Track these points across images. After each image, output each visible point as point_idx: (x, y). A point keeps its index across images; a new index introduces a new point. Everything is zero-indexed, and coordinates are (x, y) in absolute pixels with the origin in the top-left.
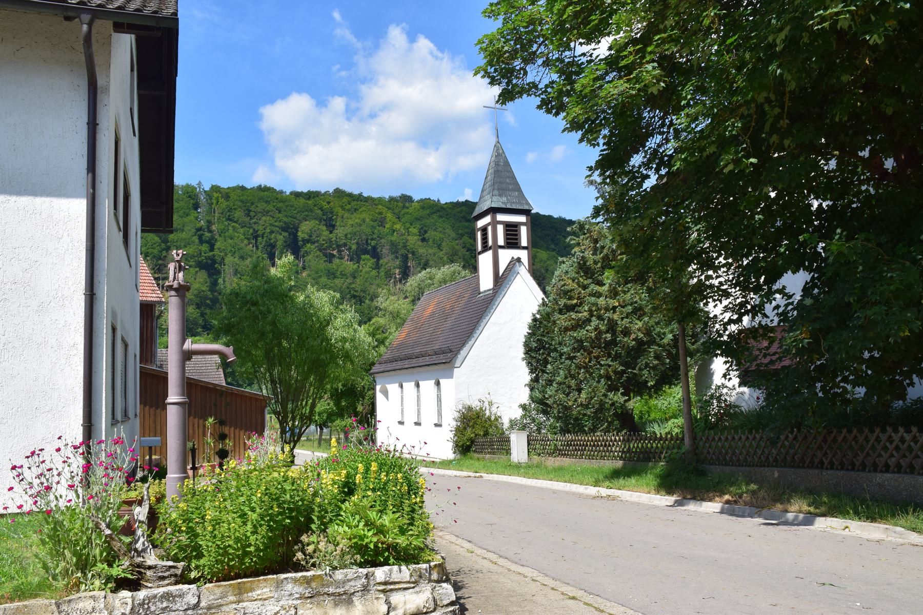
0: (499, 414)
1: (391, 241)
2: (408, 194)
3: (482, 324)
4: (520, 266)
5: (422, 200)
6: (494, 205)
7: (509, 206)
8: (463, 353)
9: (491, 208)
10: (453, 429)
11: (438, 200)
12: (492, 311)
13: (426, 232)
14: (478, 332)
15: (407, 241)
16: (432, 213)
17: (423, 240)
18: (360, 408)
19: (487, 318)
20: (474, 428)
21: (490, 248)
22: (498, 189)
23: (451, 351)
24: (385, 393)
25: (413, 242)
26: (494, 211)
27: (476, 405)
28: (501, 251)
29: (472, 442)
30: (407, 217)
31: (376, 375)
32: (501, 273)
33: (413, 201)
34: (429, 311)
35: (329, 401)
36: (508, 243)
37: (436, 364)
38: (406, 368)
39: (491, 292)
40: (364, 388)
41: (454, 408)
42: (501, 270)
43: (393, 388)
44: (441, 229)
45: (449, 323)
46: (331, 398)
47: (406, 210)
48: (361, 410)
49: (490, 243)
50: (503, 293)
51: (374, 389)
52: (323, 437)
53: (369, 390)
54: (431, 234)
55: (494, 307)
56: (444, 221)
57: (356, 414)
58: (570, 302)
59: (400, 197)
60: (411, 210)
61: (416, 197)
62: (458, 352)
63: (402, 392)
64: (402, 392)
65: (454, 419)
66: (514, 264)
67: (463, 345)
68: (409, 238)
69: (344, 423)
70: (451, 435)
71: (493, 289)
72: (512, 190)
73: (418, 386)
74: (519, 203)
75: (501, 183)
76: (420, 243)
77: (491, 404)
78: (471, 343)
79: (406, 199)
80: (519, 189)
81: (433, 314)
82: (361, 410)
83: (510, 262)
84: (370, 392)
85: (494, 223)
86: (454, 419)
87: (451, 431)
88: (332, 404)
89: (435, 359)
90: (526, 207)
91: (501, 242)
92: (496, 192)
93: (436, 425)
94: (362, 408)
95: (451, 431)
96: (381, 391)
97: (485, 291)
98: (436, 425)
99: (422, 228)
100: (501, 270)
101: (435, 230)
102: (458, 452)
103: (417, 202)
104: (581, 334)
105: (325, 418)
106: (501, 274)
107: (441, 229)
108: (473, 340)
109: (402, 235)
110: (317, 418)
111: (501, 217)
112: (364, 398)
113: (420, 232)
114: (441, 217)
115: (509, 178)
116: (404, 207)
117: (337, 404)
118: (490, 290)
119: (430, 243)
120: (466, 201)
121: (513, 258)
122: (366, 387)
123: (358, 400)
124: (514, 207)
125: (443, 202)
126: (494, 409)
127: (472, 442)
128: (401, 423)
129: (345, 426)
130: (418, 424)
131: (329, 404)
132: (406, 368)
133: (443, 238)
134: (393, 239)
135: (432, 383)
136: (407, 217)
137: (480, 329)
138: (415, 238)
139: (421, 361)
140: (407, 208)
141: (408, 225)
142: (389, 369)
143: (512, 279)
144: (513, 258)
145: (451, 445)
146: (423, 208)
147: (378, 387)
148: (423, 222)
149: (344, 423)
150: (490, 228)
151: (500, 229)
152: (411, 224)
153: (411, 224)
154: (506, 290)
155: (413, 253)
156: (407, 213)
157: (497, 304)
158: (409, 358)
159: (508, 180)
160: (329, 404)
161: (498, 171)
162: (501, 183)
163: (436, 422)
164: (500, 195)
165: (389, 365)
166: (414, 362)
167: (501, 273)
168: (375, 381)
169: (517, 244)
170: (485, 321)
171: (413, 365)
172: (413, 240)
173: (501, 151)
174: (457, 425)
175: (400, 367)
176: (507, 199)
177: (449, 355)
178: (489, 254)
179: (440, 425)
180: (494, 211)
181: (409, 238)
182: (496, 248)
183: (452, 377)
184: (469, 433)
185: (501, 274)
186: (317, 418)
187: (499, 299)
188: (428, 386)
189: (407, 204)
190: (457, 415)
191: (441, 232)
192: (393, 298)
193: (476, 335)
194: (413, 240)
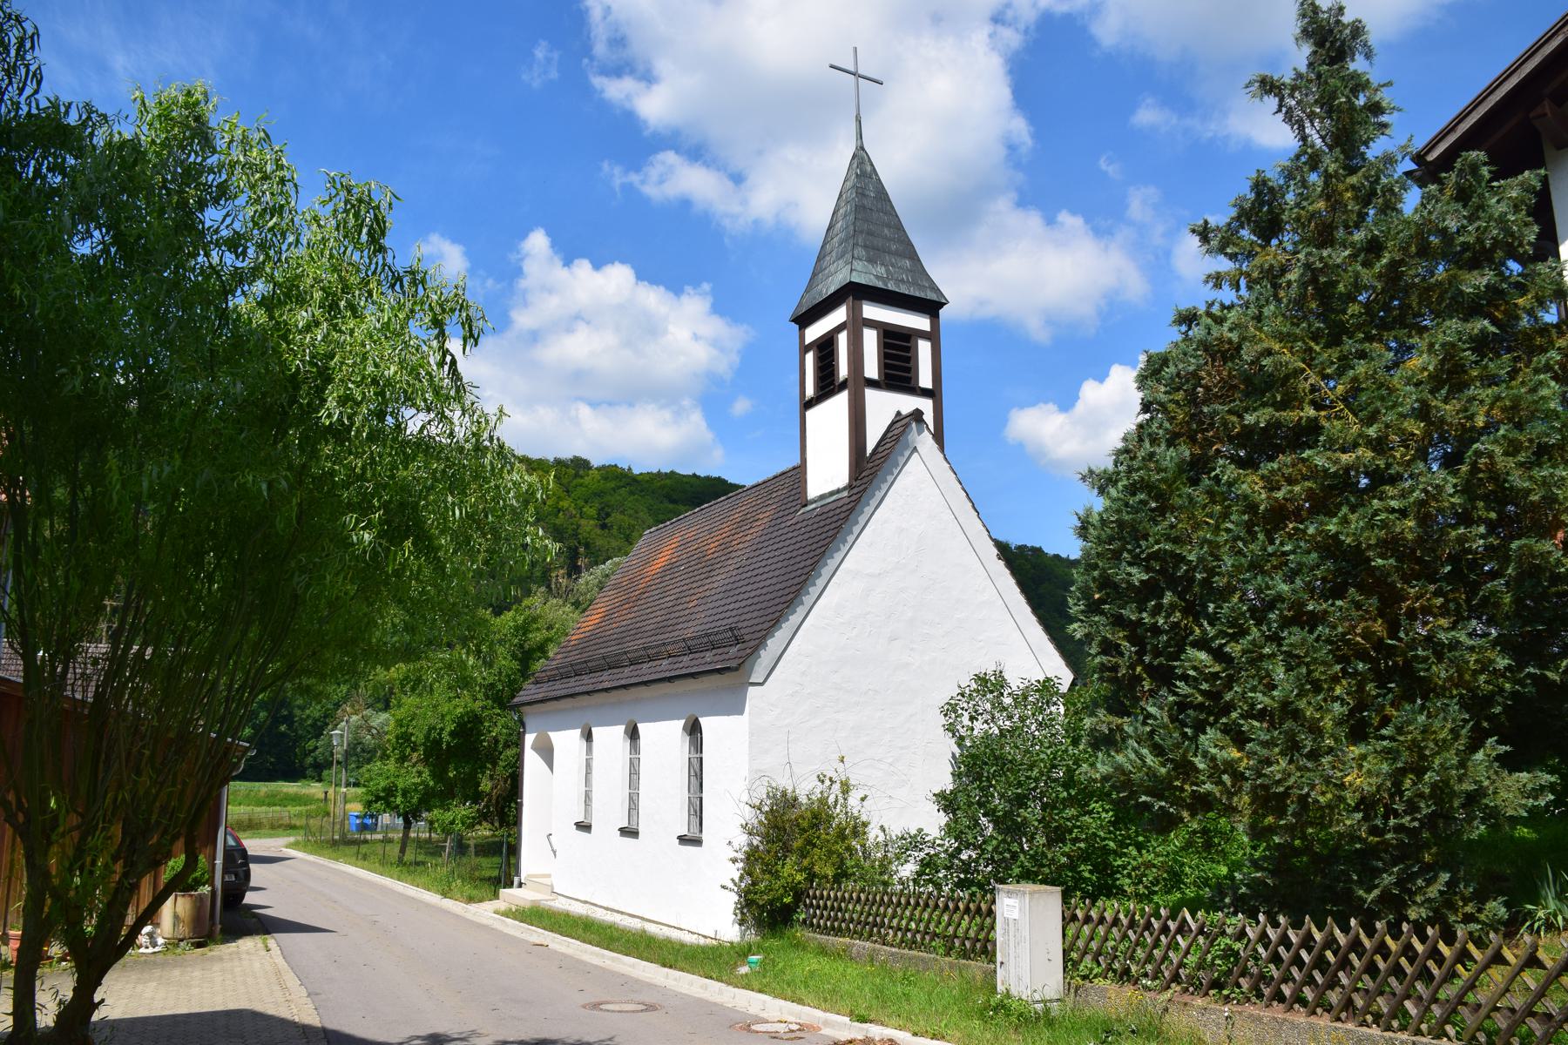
0: (864, 818)
1: (555, 525)
2: (584, 457)
3: (826, 572)
4: (920, 433)
5: (604, 467)
6: (856, 279)
7: (891, 286)
8: (774, 644)
9: (851, 283)
10: (741, 856)
11: (630, 469)
12: (850, 539)
13: (608, 515)
14: (814, 591)
15: (579, 526)
16: (619, 487)
17: (604, 527)
18: (486, 785)
19: (838, 556)
20: (804, 856)
21: (843, 386)
22: (865, 247)
23: (738, 640)
24: (547, 753)
25: (588, 529)
26: (854, 293)
27: (805, 788)
28: (871, 395)
29: (799, 895)
30: (580, 490)
31: (525, 709)
32: (870, 447)
33: (590, 468)
34: (661, 562)
35: (420, 767)
36: (887, 375)
37: (693, 675)
38: (606, 690)
39: (845, 494)
40: (496, 741)
41: (745, 798)
42: (871, 441)
43: (566, 741)
44: (631, 512)
45: (720, 579)
46: (426, 761)
47: (580, 481)
48: (488, 789)
49: (843, 371)
50: (879, 495)
51: (519, 744)
52: (413, 835)
53: (507, 746)
54: (616, 518)
55: (856, 530)
56: (637, 500)
57: (476, 797)
58: (1290, 416)
59: (572, 461)
60: (587, 480)
61: (596, 462)
62: (761, 643)
63: (589, 750)
64: (589, 750)
65: (744, 827)
66: (907, 425)
67: (775, 622)
68: (583, 522)
69: (449, 816)
70: (735, 872)
71: (850, 487)
72: (897, 254)
73: (588, 737)
74: (915, 284)
75: (870, 233)
76: (599, 531)
77: (846, 788)
78: (794, 619)
79: (580, 464)
80: (913, 256)
81: (670, 568)
82: (488, 789)
83: (893, 423)
84: (509, 752)
85: (856, 325)
86: (744, 827)
87: (734, 861)
88: (426, 774)
89: (686, 663)
90: (931, 296)
91: (872, 370)
92: (860, 252)
93: (683, 840)
94: (490, 784)
95: (734, 861)
96: (535, 748)
97: (822, 497)
98: (683, 840)
99: (602, 509)
100: (871, 441)
101: (622, 513)
102: (750, 921)
103: (598, 469)
104: (1346, 525)
105: (415, 800)
106: (869, 449)
107: (631, 512)
108: (801, 611)
109: (572, 516)
110: (399, 800)
111: (871, 311)
112: (495, 764)
113: (599, 514)
114: (632, 493)
115: (889, 226)
116: (577, 475)
117: (439, 775)
118: (838, 491)
119: (614, 531)
120: (672, 472)
121: (899, 413)
122: (502, 739)
123: (483, 768)
124: (904, 289)
125: (636, 471)
126: (853, 800)
127: (799, 895)
128: (584, 827)
129: (452, 822)
130: (629, 832)
131: (420, 773)
132: (606, 690)
133: (634, 526)
134: (558, 522)
135: (619, 730)
136: (580, 490)
137: (820, 582)
138: (592, 522)
139: (647, 671)
140: (582, 477)
141: (581, 503)
142: (558, 693)
143: (902, 460)
144: (899, 413)
145: (732, 899)
146: (606, 479)
147: (529, 739)
148: (605, 500)
149: (449, 816)
150: (843, 339)
151: (870, 338)
152: (586, 502)
153: (586, 502)
154: (884, 487)
155: (587, 546)
156: (581, 485)
157: (862, 519)
158: (612, 665)
159: (886, 231)
160: (420, 773)
161: (864, 207)
162: (870, 233)
163: (685, 832)
164: (871, 261)
165: (558, 685)
166: (627, 674)
167: (870, 447)
168: (523, 724)
169: (909, 380)
170: (832, 564)
171: (623, 682)
172: (588, 526)
173: (869, 168)
174: (750, 845)
175: (590, 688)
176: (887, 271)
177: (733, 650)
178: (841, 401)
179: (697, 842)
180: (854, 293)
181: (583, 522)
182: (858, 384)
183: (741, 712)
184: (790, 870)
185: (869, 449)
186: (399, 800)
187: (868, 510)
188: (610, 737)
189: (581, 472)
190: (749, 815)
191: (630, 516)
192: (555, 601)
193: (807, 600)
194: (588, 526)
